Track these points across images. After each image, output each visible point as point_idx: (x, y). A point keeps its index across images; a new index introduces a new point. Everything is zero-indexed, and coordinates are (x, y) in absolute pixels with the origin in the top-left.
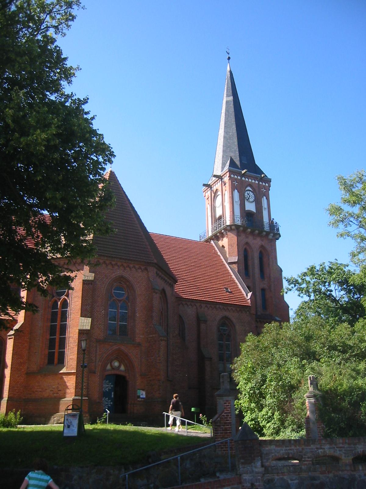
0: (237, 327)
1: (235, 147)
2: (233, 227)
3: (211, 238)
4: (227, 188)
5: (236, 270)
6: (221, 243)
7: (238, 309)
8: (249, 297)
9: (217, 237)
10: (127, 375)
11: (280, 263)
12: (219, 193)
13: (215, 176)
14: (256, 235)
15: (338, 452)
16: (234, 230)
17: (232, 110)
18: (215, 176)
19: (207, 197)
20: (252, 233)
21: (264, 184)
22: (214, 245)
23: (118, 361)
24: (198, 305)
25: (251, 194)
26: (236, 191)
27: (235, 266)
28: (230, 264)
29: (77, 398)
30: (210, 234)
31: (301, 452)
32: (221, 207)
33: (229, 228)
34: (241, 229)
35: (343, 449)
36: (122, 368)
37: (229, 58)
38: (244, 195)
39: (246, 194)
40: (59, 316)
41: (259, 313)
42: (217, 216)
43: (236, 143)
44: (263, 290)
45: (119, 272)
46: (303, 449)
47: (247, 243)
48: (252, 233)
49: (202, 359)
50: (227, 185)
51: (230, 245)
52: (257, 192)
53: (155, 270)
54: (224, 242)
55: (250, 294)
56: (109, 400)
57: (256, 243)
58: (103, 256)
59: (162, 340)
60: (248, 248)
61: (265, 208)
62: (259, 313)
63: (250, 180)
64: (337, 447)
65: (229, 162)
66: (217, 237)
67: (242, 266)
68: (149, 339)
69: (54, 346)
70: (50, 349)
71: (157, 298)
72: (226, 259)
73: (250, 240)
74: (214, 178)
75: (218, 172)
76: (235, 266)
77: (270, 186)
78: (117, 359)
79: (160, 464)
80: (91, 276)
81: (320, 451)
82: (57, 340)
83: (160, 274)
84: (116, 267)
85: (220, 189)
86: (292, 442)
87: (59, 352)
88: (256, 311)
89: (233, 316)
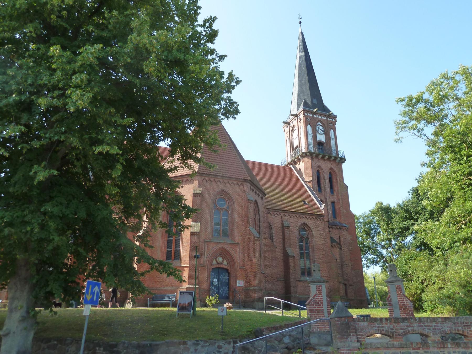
0: (314, 232)
1: (308, 92)
2: (308, 154)
3: (290, 163)
4: (302, 124)
5: (311, 187)
6: (298, 166)
7: (314, 218)
8: (322, 208)
9: (294, 162)
10: (229, 268)
11: (346, 181)
12: (296, 128)
13: (292, 115)
14: (326, 159)
15: (427, 330)
16: (308, 156)
17: (304, 69)
18: (292, 115)
19: (286, 132)
20: (323, 157)
21: (331, 120)
22: (293, 168)
23: (222, 257)
24: (282, 214)
25: (321, 128)
26: (309, 126)
27: (310, 184)
28: (305, 182)
29: (190, 286)
30: (289, 160)
31: (392, 329)
32: (298, 138)
33: (304, 155)
34: (314, 155)
35: (431, 328)
36: (225, 263)
37: (300, 23)
38: (316, 129)
39: (317, 128)
40: (173, 244)
41: (330, 221)
42: (295, 147)
43: (308, 88)
44: (333, 203)
45: (221, 187)
46: (394, 327)
47: (319, 166)
48: (323, 157)
49: (286, 258)
50: (302, 121)
51: (306, 168)
52: (326, 125)
53: (249, 185)
54: (301, 166)
55: (323, 206)
56: (223, 280)
57: (326, 166)
58: (209, 174)
59: (256, 240)
60: (320, 170)
61: (333, 139)
62: (330, 221)
63: (320, 117)
64: (426, 326)
65: (303, 103)
66: (294, 162)
67: (316, 185)
68: (246, 239)
69: (172, 245)
70: (168, 238)
71: (252, 206)
72: (303, 181)
73: (322, 163)
74: (291, 117)
75: (295, 112)
76: (310, 184)
77: (336, 121)
78: (221, 255)
79: (262, 338)
80: (199, 191)
81: (409, 328)
82: (174, 241)
83: (253, 188)
84: (219, 183)
85: (296, 125)
86: (384, 320)
87: (175, 250)
88: (328, 219)
89: (310, 222)
